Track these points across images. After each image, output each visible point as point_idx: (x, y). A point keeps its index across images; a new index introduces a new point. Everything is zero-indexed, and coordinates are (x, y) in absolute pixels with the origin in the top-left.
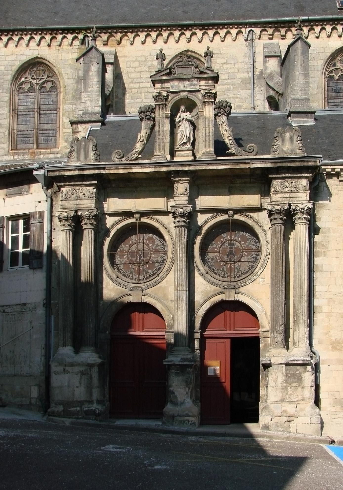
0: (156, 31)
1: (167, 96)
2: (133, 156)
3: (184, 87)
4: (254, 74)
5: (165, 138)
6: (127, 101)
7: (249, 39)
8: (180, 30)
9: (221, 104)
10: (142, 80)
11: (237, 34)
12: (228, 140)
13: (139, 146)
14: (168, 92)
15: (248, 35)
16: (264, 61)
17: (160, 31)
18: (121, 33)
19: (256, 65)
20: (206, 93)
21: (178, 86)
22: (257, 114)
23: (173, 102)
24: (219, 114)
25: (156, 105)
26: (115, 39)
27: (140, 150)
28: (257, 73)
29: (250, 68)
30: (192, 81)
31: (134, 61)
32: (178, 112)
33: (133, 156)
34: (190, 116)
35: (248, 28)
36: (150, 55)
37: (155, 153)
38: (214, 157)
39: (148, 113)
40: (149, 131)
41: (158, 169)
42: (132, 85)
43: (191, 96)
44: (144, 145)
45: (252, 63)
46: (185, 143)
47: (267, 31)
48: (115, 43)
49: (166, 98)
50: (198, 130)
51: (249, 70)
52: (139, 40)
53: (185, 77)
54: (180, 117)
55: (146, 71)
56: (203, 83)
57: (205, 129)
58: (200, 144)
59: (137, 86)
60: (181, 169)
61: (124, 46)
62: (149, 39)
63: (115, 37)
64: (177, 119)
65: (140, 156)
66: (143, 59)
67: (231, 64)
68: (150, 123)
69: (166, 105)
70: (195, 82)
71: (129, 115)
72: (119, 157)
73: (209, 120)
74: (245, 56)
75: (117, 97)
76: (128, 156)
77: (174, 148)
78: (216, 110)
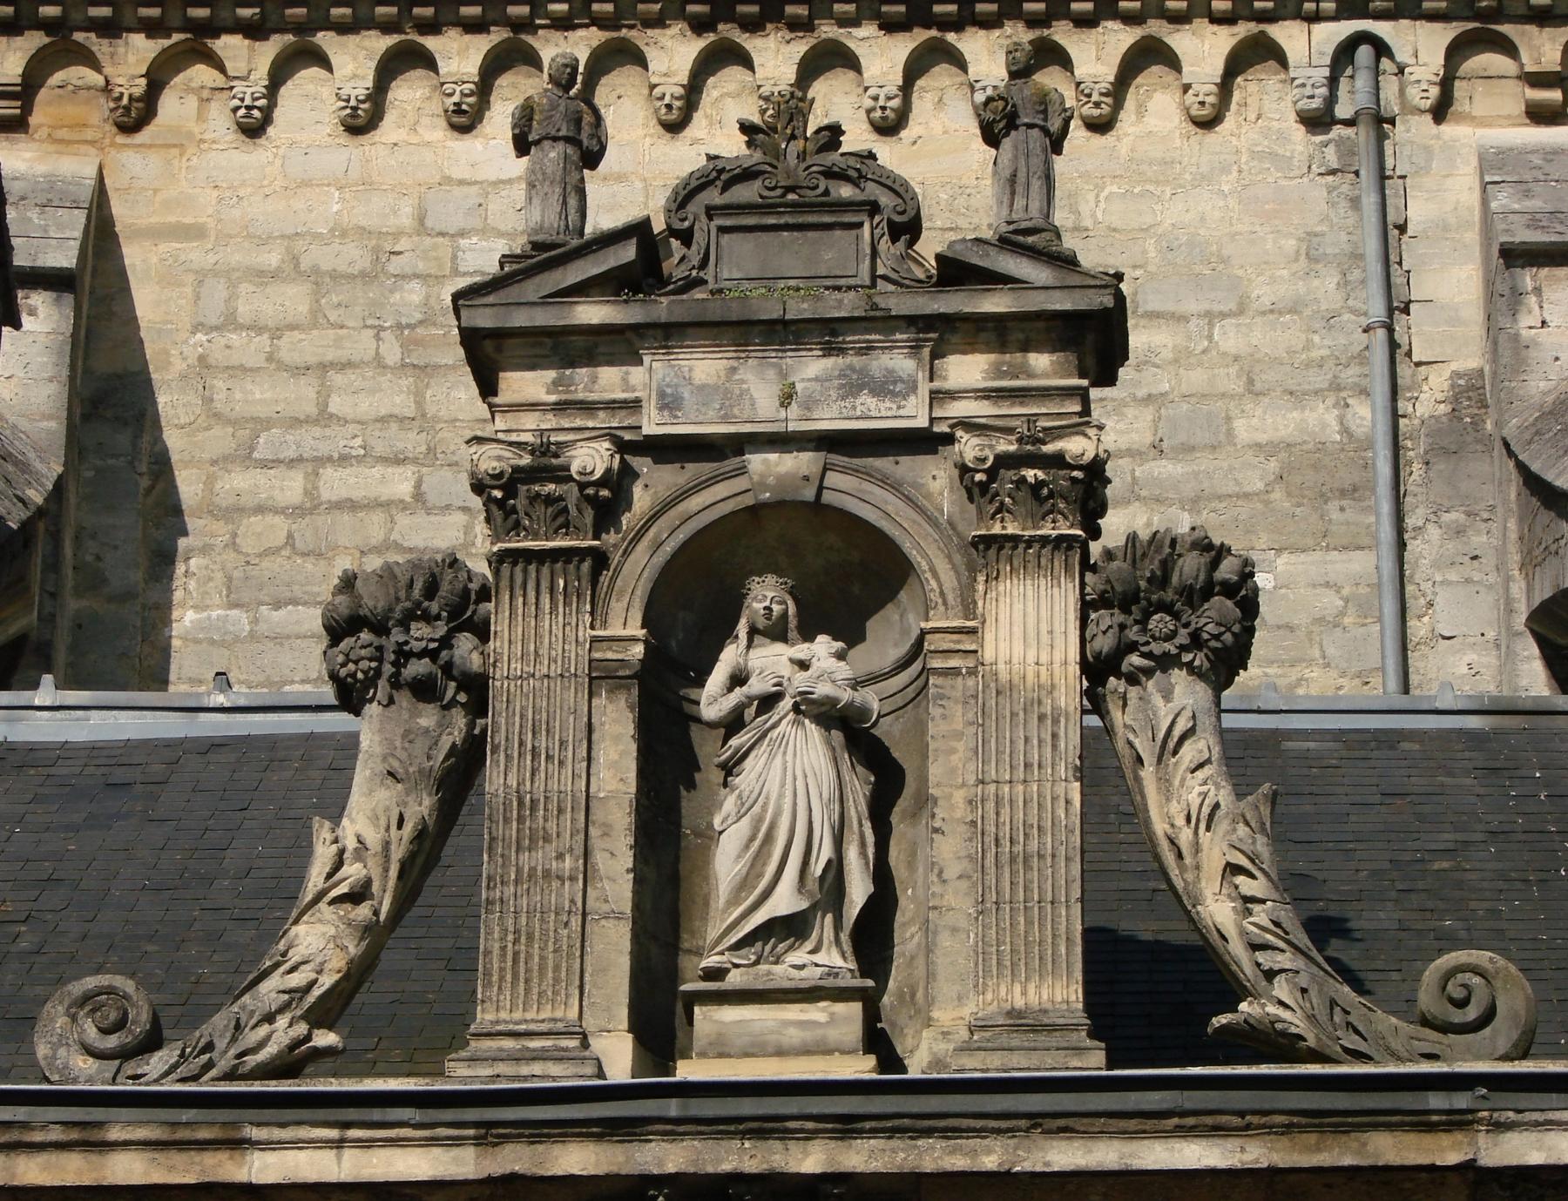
0: (475, 27)
1: (619, 482)
2: (252, 1037)
3: (787, 398)
4: (1395, 416)
5: (588, 873)
6: (185, 619)
7: (1343, 110)
8: (699, 26)
9: (1151, 566)
10: (340, 440)
11: (1236, 65)
12: (1227, 908)
13: (318, 944)
14: (622, 447)
15: (1333, 81)
16: (1490, 295)
17: (519, 26)
18: (152, 29)
19: (1420, 333)
20: (1003, 461)
21: (725, 395)
22: (1473, 722)
23: (669, 537)
24: (1135, 659)
25: (498, 560)
26: (97, 79)
27: (327, 981)
28: (1428, 399)
29: (1362, 357)
30: (868, 349)
31: (264, 277)
32: (725, 633)
33: (252, 1037)
34: (843, 670)
35: (1335, 18)
36: (421, 225)
37: (485, 1017)
38: (1093, 1062)
39: (419, 630)
40: (422, 806)
41: (515, 1159)
42: (238, 482)
43: (851, 490)
44: (376, 935)
45: (1378, 311)
46: (791, 928)
47: (1509, 48)
48: (98, 113)
49: (609, 495)
50: (924, 801)
51: (1350, 375)
52: (311, 102)
53: (800, 309)
54: (738, 679)
55: (379, 362)
56: (968, 369)
57: (999, 786)
58: (945, 941)
59: (291, 487)
60: (751, 1166)
61: (179, 144)
62: (408, 92)
63: (97, 68)
64: (713, 699)
65: (325, 1038)
66: (354, 256)
67: (1183, 319)
68: (443, 726)
69: (600, 560)
70: (900, 362)
71: (220, 699)
72: (112, 1042)
73: (1036, 707)
74: (1312, 254)
75: (92, 581)
76: (203, 1033)
77: (673, 975)
78: (1103, 619)
